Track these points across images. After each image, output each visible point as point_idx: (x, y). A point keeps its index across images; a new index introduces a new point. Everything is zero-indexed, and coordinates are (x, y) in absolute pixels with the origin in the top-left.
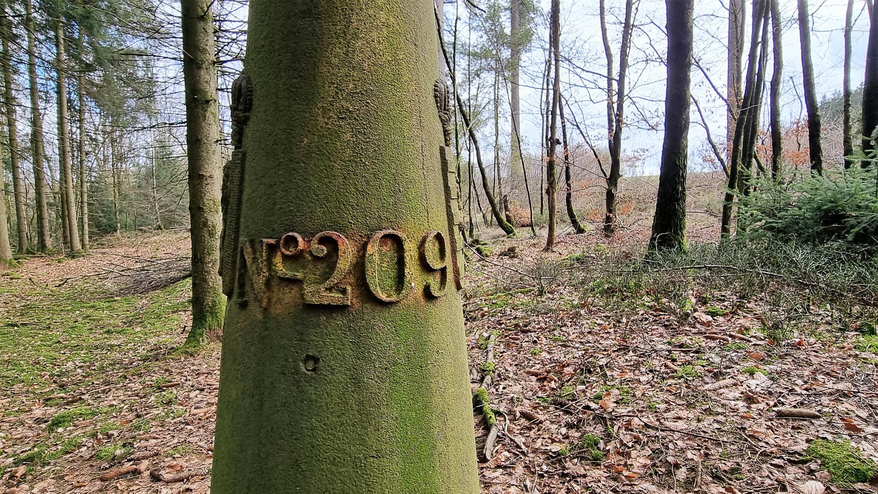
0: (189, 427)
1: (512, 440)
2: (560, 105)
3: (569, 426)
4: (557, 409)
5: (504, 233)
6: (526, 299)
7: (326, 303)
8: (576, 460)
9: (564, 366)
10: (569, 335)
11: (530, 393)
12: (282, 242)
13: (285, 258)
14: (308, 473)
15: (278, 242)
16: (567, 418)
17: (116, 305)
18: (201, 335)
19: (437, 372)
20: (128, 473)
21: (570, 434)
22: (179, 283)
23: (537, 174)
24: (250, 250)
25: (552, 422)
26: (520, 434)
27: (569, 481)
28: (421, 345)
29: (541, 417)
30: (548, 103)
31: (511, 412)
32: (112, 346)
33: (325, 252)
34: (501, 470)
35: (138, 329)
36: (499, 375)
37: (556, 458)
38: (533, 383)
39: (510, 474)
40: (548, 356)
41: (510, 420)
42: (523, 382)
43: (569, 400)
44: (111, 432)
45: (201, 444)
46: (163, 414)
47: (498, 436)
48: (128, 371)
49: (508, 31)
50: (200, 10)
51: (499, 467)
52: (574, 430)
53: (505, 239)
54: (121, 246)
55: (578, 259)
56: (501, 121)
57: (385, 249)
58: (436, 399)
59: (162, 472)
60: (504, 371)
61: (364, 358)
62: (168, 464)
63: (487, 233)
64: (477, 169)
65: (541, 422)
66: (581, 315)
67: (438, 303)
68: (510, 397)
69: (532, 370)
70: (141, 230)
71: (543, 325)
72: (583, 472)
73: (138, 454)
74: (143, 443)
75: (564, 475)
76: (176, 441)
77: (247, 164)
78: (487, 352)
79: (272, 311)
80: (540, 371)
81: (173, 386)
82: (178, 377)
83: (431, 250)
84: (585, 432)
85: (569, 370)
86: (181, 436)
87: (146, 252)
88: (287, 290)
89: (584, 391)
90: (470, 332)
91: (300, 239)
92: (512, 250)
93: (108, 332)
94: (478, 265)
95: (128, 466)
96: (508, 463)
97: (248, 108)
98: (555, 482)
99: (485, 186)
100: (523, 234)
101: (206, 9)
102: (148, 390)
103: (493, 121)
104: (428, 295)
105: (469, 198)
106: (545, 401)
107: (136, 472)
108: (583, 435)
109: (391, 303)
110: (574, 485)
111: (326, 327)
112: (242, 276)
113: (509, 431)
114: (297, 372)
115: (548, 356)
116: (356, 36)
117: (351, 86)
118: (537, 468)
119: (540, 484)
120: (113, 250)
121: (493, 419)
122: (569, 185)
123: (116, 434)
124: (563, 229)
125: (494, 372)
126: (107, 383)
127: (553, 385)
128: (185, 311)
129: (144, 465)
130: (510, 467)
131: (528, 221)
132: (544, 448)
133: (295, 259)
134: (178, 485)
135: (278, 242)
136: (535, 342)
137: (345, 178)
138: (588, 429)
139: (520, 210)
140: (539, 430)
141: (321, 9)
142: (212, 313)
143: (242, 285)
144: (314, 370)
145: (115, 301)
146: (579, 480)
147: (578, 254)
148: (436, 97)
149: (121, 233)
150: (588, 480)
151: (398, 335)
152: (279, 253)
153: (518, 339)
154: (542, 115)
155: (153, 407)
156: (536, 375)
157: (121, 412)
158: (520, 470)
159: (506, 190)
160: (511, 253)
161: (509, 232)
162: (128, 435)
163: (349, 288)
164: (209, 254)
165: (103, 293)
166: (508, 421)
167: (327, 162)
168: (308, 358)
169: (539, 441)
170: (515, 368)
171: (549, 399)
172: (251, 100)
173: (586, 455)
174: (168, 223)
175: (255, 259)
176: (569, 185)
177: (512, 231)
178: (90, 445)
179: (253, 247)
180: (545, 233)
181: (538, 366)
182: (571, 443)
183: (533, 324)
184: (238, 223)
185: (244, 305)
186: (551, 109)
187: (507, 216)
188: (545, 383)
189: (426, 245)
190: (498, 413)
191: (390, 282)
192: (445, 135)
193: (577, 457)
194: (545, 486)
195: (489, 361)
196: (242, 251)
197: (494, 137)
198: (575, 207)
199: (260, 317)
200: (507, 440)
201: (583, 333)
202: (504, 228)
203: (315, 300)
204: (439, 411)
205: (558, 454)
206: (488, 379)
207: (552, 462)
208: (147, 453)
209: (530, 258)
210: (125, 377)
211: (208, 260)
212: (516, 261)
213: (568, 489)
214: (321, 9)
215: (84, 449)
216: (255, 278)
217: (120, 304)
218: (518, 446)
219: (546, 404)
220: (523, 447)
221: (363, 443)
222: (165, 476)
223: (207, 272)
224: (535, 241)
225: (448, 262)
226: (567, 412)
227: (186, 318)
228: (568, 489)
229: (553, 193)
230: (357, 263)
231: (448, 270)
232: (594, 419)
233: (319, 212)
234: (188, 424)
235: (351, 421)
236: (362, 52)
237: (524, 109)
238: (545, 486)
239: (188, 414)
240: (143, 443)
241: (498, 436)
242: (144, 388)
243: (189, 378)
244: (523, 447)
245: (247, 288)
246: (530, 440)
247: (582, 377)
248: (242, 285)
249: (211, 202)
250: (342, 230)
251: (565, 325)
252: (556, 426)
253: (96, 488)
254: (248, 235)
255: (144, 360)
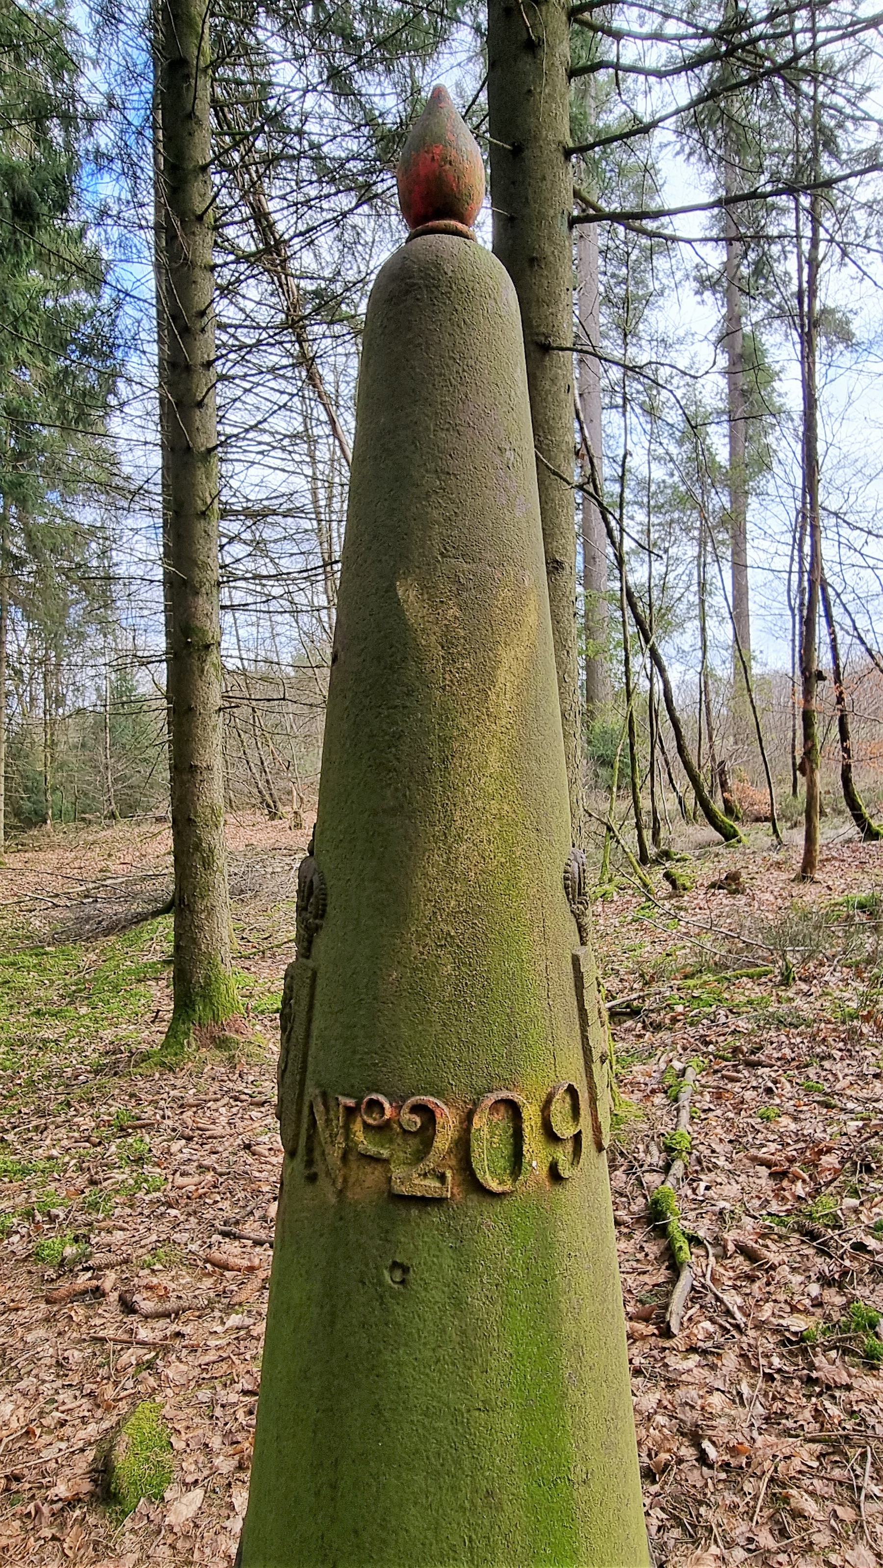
0: (173, 1212)
1: (718, 1299)
2: (826, 600)
3: (826, 1281)
4: (803, 1242)
5: (718, 836)
6: (756, 992)
7: (419, 1194)
8: (833, 1354)
9: (821, 1152)
10: (837, 1079)
11: (757, 1203)
12: (363, 1106)
13: (367, 1126)
14: (393, 1425)
15: (358, 1104)
16: (821, 1264)
17: (48, 962)
18: (187, 1035)
19: (569, 1285)
20: (85, 1292)
21: (826, 1299)
22: (147, 926)
23: (782, 734)
24: (322, 1108)
25: (794, 1270)
26: (734, 1287)
27: (820, 1394)
28: (545, 1247)
29: (774, 1258)
30: (801, 591)
31: (718, 1241)
32: (45, 1041)
33: (419, 1125)
34: (697, 1357)
35: (84, 1011)
36: (699, 1161)
37: (798, 1345)
38: (763, 1182)
39: (713, 1367)
40: (793, 1126)
41: (716, 1257)
42: (743, 1178)
43: (827, 1226)
44: (54, 1211)
45: (194, 1247)
46: (131, 1182)
47: (693, 1288)
48: (74, 1092)
49: (722, 455)
50: (199, 502)
51: (693, 1349)
52: (833, 1290)
53: (720, 849)
54: (52, 847)
55: (862, 907)
56: (710, 623)
57: (496, 1118)
58: (568, 1327)
59: (137, 1298)
60: (707, 1152)
61: (468, 1270)
62: (144, 1282)
63: (687, 835)
64: (664, 714)
65: (773, 1268)
66: (862, 1034)
67: (568, 1185)
68: (717, 1209)
69: (760, 1155)
70: (84, 819)
71: (787, 1051)
72: (844, 1379)
73: (99, 1258)
74: (105, 1238)
75: (810, 1381)
76: (154, 1238)
77: (318, 989)
78: (678, 1110)
79: (349, 1194)
80: (776, 1158)
81: (142, 1127)
82: (150, 1110)
83: (560, 1108)
84: (853, 1300)
85: (830, 1160)
86: (162, 1228)
87: (94, 859)
88: (369, 1169)
89: (856, 1211)
90: (650, 1056)
91: (387, 1105)
92: (733, 877)
93: (38, 1013)
94: (668, 906)
95: (83, 1280)
96: (709, 1344)
97: (321, 914)
98: (795, 1392)
99: (681, 749)
100: (755, 836)
101: (209, 501)
102: (105, 1132)
103: (697, 623)
104: (555, 1176)
105: (652, 771)
106: (782, 1223)
107: (98, 1293)
108: (849, 1302)
109: (504, 1194)
110: (827, 1404)
111: (418, 1225)
112: (310, 1138)
113: (713, 1279)
114: (381, 1283)
115: (793, 1126)
116: (459, 838)
117: (453, 903)
118: (763, 1361)
119: (766, 1395)
120: (41, 855)
121: (686, 1253)
122: (846, 750)
123: (62, 1216)
124: (835, 830)
125: (690, 1153)
126: (41, 1113)
127: (799, 1189)
128: (157, 979)
129: (109, 1280)
130: (712, 1353)
131: (765, 810)
132: (775, 1321)
133: (382, 1130)
134: (162, 1323)
135: (358, 1104)
136: (769, 1091)
137: (445, 1024)
138: (860, 1291)
139: (750, 790)
140: (768, 1284)
141: (415, 805)
142: (204, 997)
143: (310, 1150)
144: (403, 1282)
145: (46, 954)
146: (837, 1394)
147: (861, 895)
148: (566, 887)
149: (53, 826)
150: (854, 1396)
151: (514, 1237)
152: (359, 1119)
153: (738, 1080)
154: (792, 609)
155: (111, 1166)
156: (768, 1164)
157: (65, 1171)
158: (730, 1360)
159: (724, 746)
160: (731, 883)
161: (729, 835)
162: (81, 1218)
163: (449, 1174)
164: (203, 898)
165: (28, 938)
166: (712, 1259)
167: (422, 1003)
168: (395, 1265)
169: (768, 1307)
170: (729, 1147)
171: (791, 1220)
172: (325, 905)
173: (852, 1345)
174: (128, 808)
175: (328, 1121)
176: (846, 750)
177: (735, 834)
178: (24, 1231)
179: (325, 1104)
180: (798, 837)
181: (773, 1147)
182: (828, 1318)
183: (769, 1050)
184: (305, 1061)
185: (312, 1178)
186: (806, 602)
187: (726, 801)
188: (785, 1183)
189: (552, 1108)
190: (695, 1241)
191: (502, 1163)
192: (580, 931)
193: (837, 1348)
194: (774, 1398)
195: (681, 1130)
196: (311, 1107)
197: (700, 654)
198: (858, 786)
199: (333, 1200)
200: (710, 1299)
201: (862, 1076)
202: (718, 828)
203: (405, 1190)
204: (571, 1342)
205: (801, 1337)
206: (678, 1168)
207: (790, 1352)
208: (112, 1258)
209: (768, 896)
210: (69, 1105)
211: (200, 906)
212: (742, 900)
213: (816, 1410)
214: (415, 805)
215: (15, 1238)
216: (328, 1149)
217: (55, 962)
218: (728, 1313)
219: (784, 1230)
220: (738, 1315)
221: (466, 1389)
222: (143, 1304)
223: (197, 927)
224: (777, 857)
225: (585, 1123)
226: (822, 1252)
227: (160, 994)
228: (816, 1410)
229: (812, 771)
230: (460, 1138)
231: (583, 1136)
232: (872, 1271)
233: (411, 1069)
234: (170, 1206)
235: (450, 1356)
236: (467, 858)
237: (779, 509)
238: (774, 1398)
239: (169, 1186)
240: (105, 1238)
241: (693, 1288)
242: (98, 1127)
243: (168, 1113)
244: (738, 1315)
245: (317, 1155)
246: (752, 1302)
247: (854, 1180)
248: (310, 1150)
249: (208, 810)
250: (439, 1094)
251: (830, 1056)
252: (800, 1278)
253: (40, 1315)
254: (318, 1085)
255: (97, 1072)
